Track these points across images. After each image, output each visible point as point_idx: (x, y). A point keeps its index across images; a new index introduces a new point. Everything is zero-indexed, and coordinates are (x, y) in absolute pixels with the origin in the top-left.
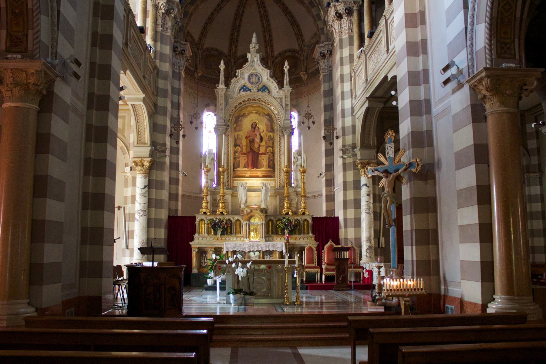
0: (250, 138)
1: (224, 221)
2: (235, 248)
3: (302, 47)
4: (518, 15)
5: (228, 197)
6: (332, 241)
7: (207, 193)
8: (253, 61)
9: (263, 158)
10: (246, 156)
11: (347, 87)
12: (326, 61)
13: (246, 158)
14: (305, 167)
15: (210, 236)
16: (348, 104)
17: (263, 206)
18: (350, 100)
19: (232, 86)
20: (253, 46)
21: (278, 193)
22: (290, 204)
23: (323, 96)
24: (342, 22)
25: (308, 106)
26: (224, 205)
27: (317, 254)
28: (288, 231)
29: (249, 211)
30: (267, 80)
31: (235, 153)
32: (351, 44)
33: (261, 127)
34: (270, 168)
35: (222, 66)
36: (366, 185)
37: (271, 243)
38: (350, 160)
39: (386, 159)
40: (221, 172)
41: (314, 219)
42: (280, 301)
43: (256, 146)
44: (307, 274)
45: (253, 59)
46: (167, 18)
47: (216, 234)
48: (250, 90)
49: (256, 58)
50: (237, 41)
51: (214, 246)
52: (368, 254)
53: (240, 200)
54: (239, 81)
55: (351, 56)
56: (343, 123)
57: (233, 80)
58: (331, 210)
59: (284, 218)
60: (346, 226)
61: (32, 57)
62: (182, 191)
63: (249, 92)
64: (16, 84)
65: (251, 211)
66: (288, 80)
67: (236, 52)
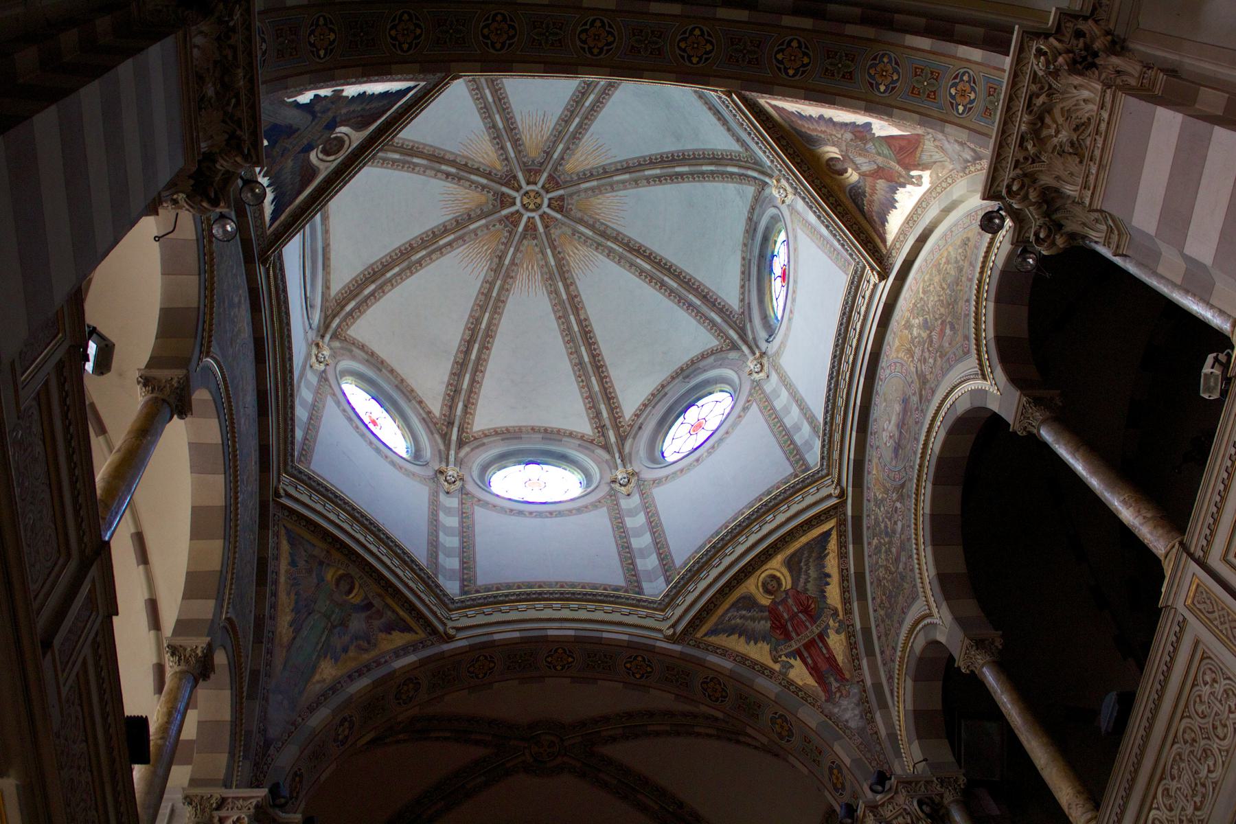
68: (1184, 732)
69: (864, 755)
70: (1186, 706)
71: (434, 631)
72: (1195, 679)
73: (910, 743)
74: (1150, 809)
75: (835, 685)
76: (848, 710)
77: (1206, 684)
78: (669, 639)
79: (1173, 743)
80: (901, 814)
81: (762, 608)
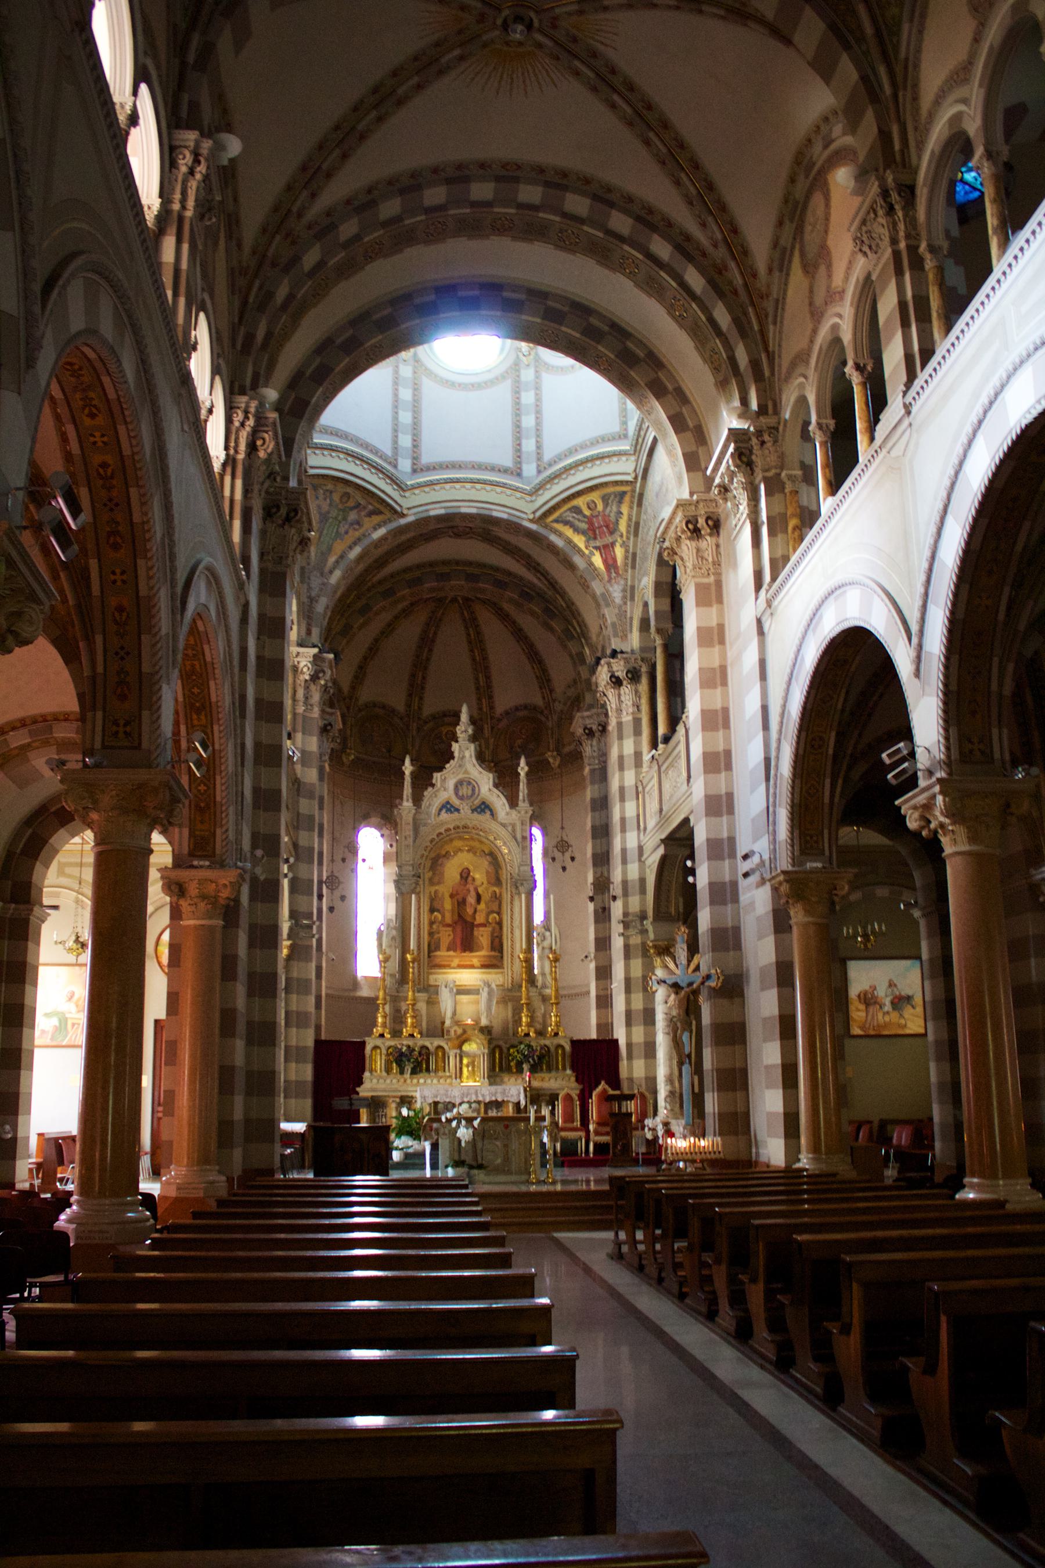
4: (827, 800)
5: (422, 1006)
6: (606, 1083)
8: (463, 757)
11: (631, 808)
12: (595, 743)
14: (558, 952)
15: (392, 1076)
16: (632, 840)
17: (484, 1022)
18: (635, 833)
21: (510, 996)
22: (532, 1018)
23: (589, 808)
24: (622, 692)
25: (562, 828)
29: (460, 1031)
32: (637, 732)
33: (477, 876)
35: (408, 768)
37: (499, 1088)
38: (636, 940)
39: (677, 966)
41: (574, 1043)
42: (524, 1178)
44: (564, 1141)
46: (313, 687)
47: (402, 1072)
48: (458, 810)
50: (423, 688)
51: (399, 1094)
53: (443, 1011)
55: (638, 755)
56: (624, 873)
57: (428, 792)
58: (605, 1026)
59: (521, 1043)
60: (630, 1057)
61: (222, 865)
62: (327, 987)
63: (456, 813)
64: (203, 897)
65: (465, 1032)
66: (526, 791)
67: (420, 708)
71: (395, 511)
75: (614, 575)
76: (616, 592)
78: (531, 521)
81: (585, 516)
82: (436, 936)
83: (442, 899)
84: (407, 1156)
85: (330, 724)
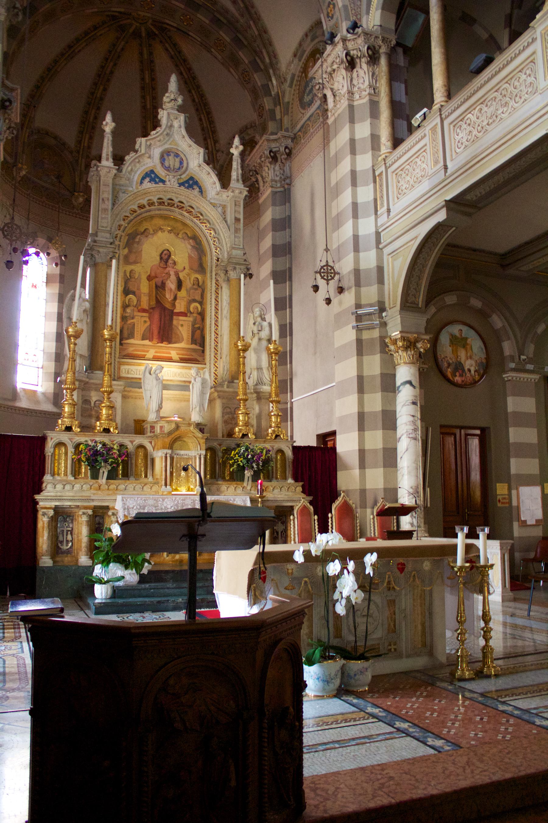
0: (157, 279)
1: (115, 447)
2: (144, 509)
3: (212, 152)
5: (117, 398)
7: (74, 384)
8: (171, 126)
9: (181, 323)
10: (147, 315)
13: (147, 319)
17: (195, 417)
19: (126, 168)
20: (172, 97)
26: (110, 412)
27: (318, 522)
28: (252, 473)
30: (197, 168)
31: (125, 307)
34: (196, 344)
36: (410, 383)
40: (105, 340)
41: (296, 450)
43: (168, 296)
45: (171, 122)
47: (95, 476)
48: (163, 182)
49: (177, 121)
52: (414, 520)
54: (141, 160)
63: (161, 184)
67: (89, 147)
68: (503, 89)
69: (350, 4)
70: (511, 78)
72: (523, 69)
73: (377, 9)
74: (470, 113)
77: (525, 74)
79: (496, 91)
80: (356, 49)
82: (130, 321)
83: (139, 278)
84: (116, 593)
85: (10, 101)
